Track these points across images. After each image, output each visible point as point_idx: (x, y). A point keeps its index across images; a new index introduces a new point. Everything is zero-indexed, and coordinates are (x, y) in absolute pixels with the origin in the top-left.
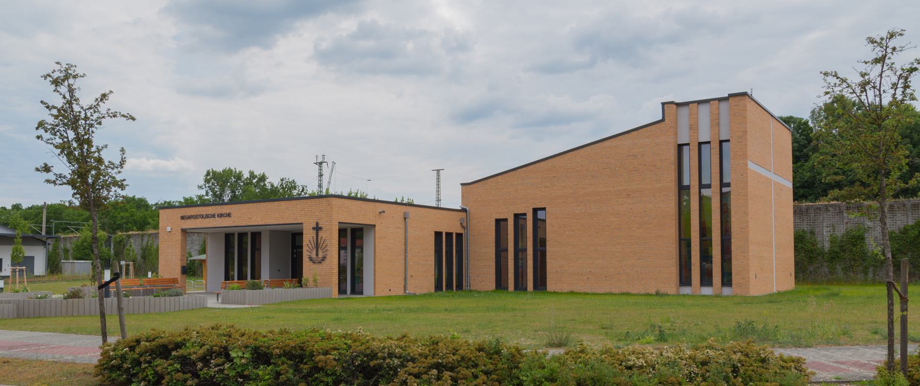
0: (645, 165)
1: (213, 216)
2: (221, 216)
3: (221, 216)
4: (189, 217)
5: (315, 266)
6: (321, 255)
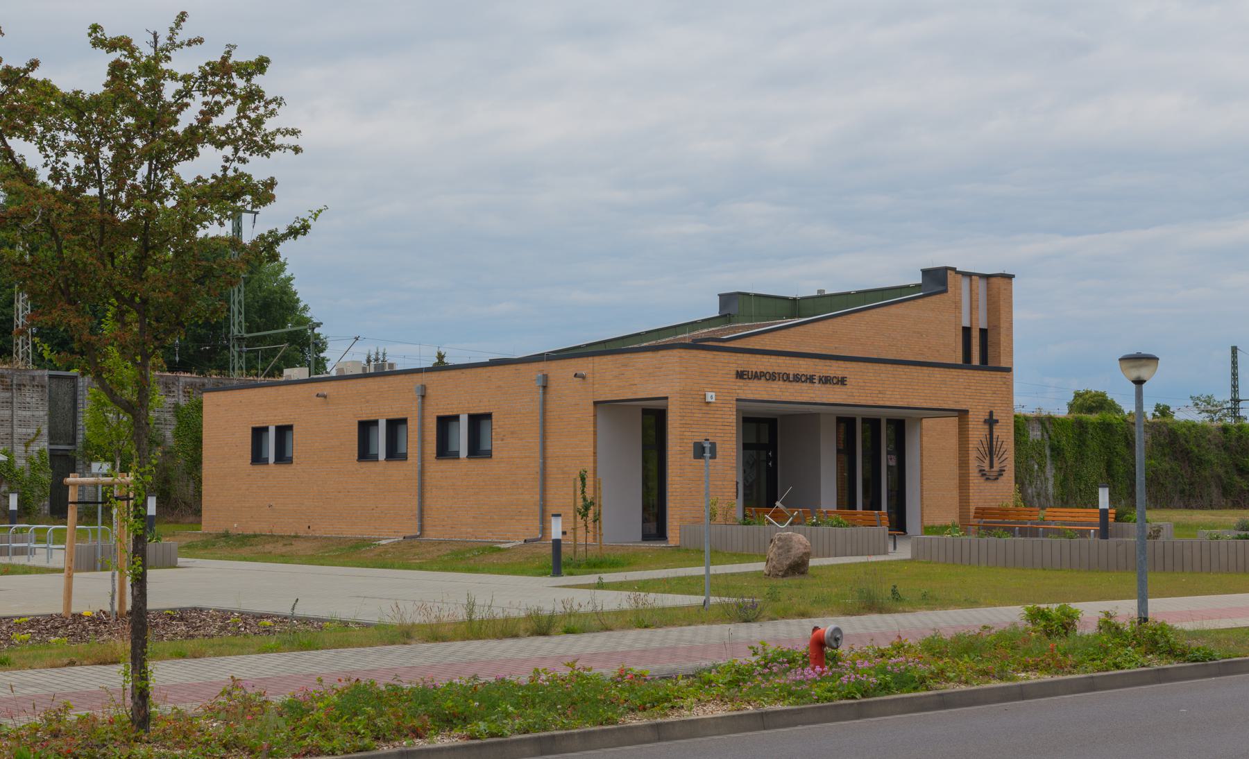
0: (930, 348)
1: (810, 379)
2: (826, 380)
3: (826, 380)
4: (758, 376)
5: (989, 484)
6: (996, 467)
